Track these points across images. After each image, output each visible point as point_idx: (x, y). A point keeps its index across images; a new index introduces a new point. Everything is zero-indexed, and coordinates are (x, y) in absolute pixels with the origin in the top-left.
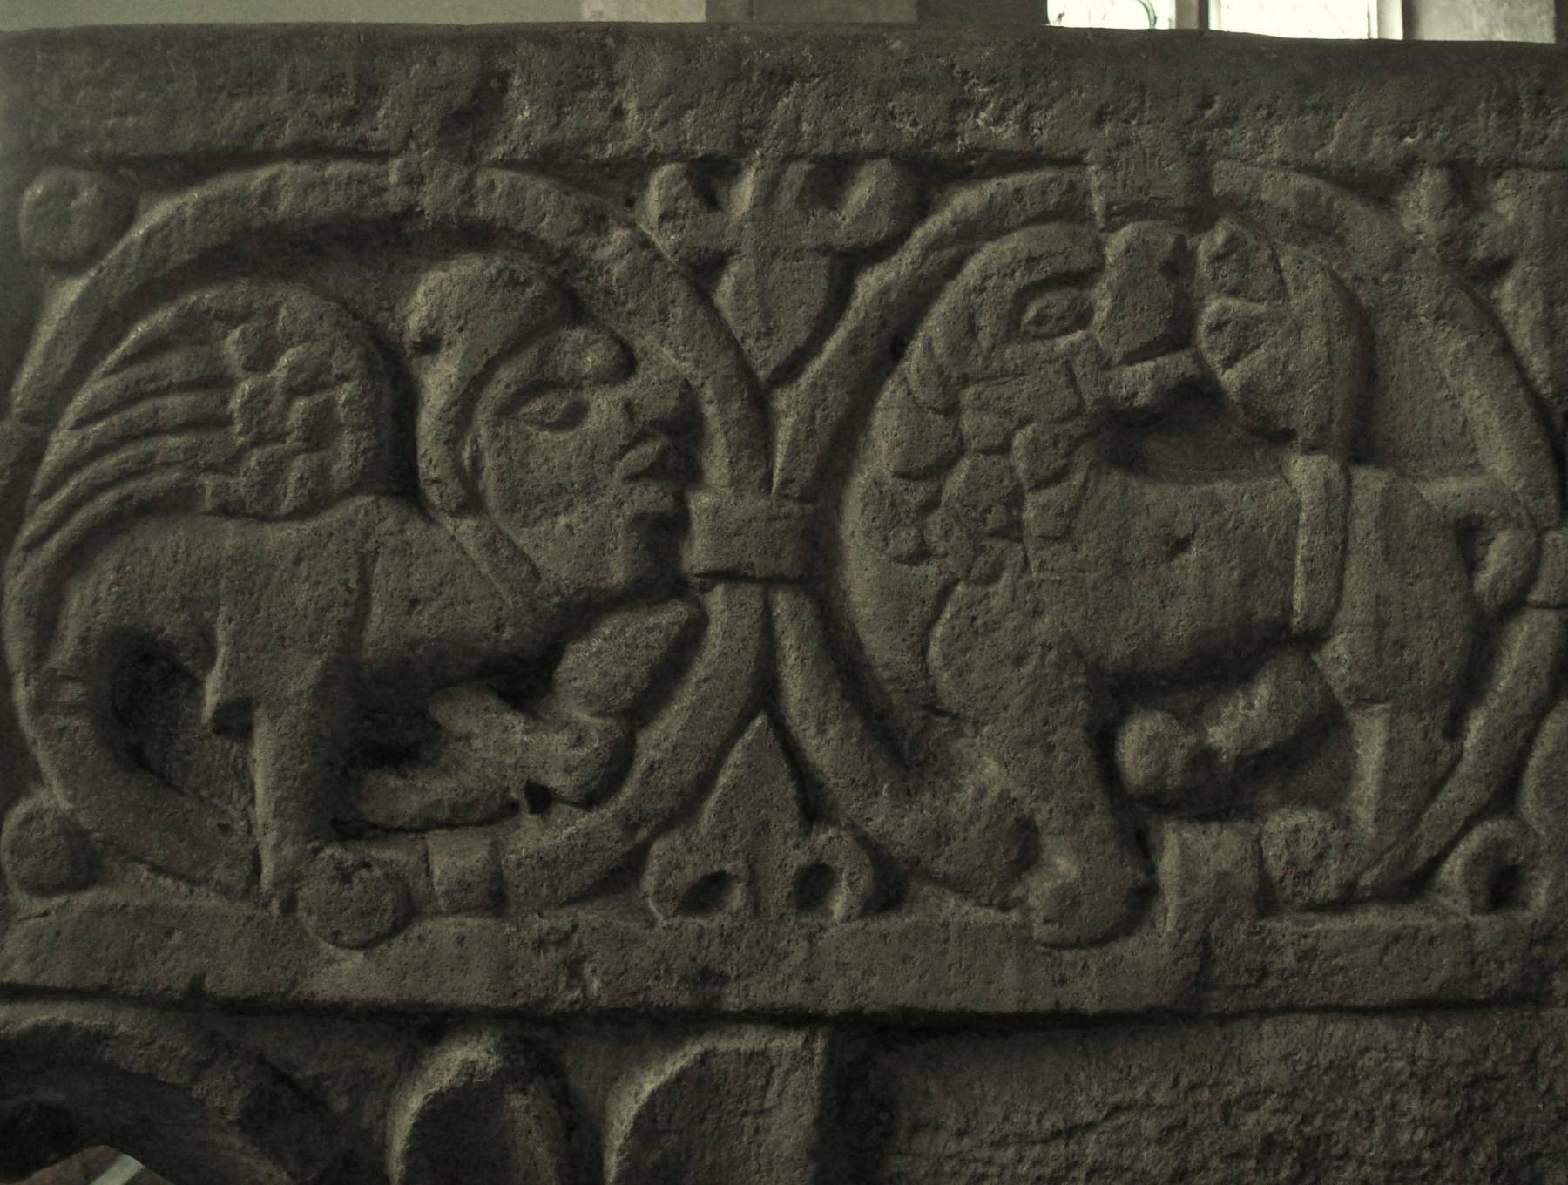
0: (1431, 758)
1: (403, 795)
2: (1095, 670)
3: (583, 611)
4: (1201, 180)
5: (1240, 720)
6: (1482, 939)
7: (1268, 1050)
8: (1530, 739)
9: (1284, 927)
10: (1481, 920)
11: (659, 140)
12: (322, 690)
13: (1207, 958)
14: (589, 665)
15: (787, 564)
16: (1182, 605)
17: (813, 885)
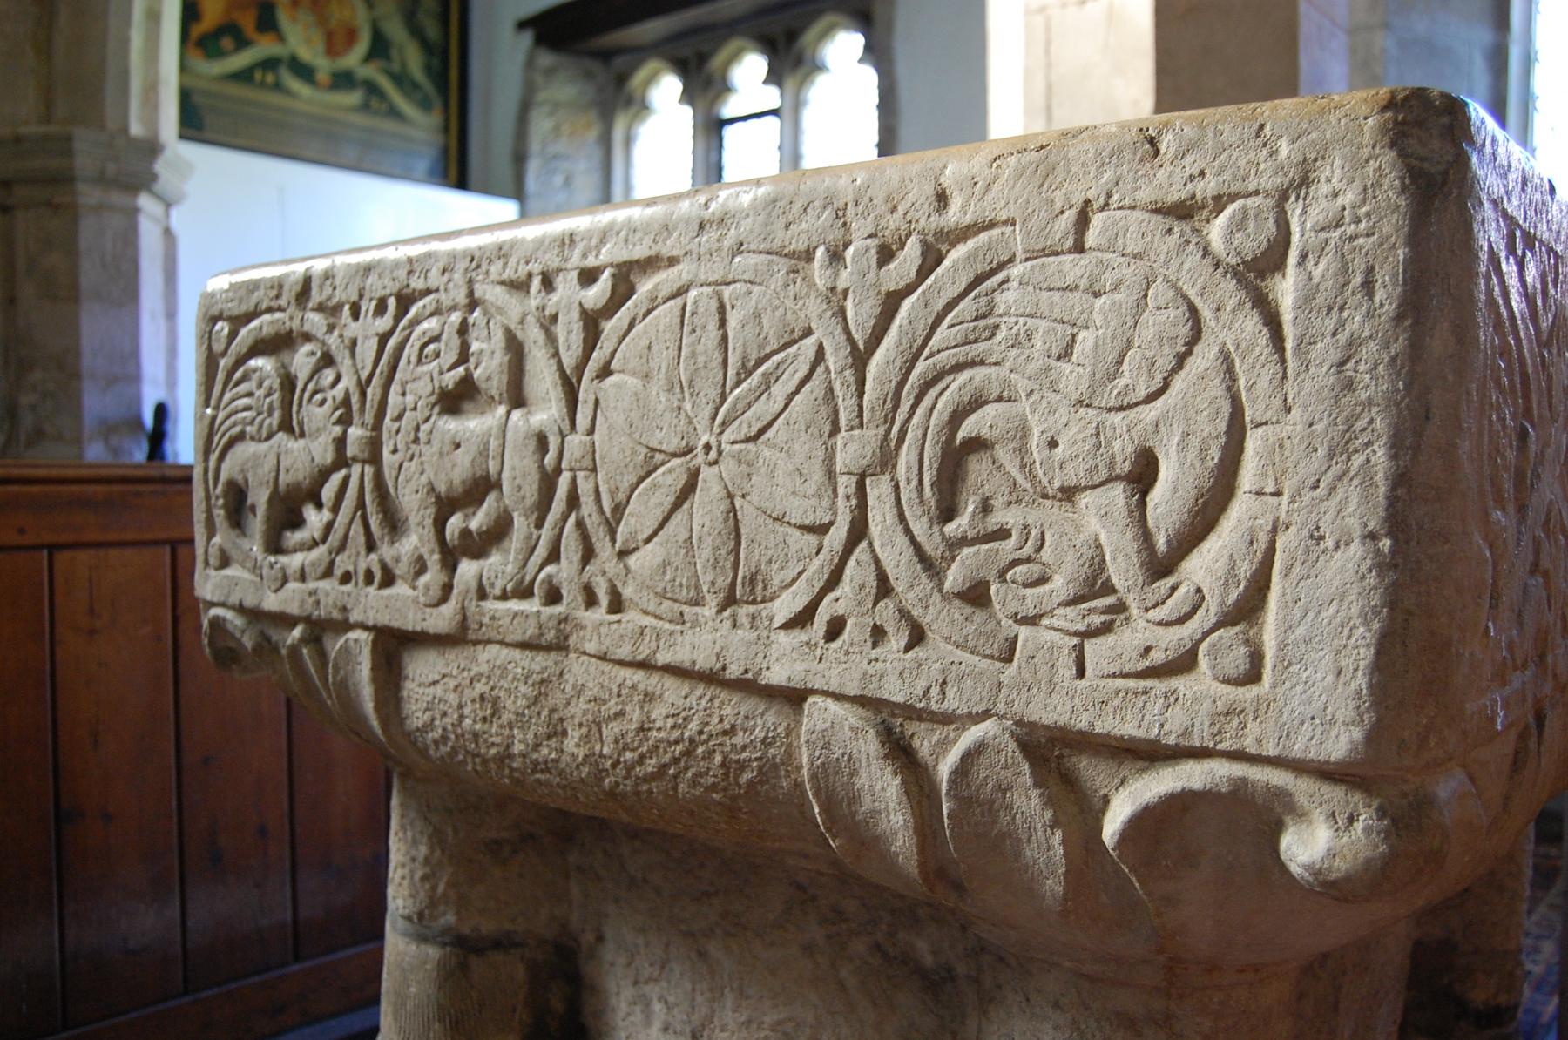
0: (529, 536)
1: (294, 537)
2: (438, 497)
3: (324, 475)
4: (471, 293)
5: (478, 520)
6: (543, 618)
7: (490, 655)
8: (562, 529)
9: (490, 605)
10: (543, 609)
11: (344, 298)
12: (270, 501)
13: (465, 618)
14: (328, 492)
15: (366, 455)
16: (459, 469)
17: (878, 634)
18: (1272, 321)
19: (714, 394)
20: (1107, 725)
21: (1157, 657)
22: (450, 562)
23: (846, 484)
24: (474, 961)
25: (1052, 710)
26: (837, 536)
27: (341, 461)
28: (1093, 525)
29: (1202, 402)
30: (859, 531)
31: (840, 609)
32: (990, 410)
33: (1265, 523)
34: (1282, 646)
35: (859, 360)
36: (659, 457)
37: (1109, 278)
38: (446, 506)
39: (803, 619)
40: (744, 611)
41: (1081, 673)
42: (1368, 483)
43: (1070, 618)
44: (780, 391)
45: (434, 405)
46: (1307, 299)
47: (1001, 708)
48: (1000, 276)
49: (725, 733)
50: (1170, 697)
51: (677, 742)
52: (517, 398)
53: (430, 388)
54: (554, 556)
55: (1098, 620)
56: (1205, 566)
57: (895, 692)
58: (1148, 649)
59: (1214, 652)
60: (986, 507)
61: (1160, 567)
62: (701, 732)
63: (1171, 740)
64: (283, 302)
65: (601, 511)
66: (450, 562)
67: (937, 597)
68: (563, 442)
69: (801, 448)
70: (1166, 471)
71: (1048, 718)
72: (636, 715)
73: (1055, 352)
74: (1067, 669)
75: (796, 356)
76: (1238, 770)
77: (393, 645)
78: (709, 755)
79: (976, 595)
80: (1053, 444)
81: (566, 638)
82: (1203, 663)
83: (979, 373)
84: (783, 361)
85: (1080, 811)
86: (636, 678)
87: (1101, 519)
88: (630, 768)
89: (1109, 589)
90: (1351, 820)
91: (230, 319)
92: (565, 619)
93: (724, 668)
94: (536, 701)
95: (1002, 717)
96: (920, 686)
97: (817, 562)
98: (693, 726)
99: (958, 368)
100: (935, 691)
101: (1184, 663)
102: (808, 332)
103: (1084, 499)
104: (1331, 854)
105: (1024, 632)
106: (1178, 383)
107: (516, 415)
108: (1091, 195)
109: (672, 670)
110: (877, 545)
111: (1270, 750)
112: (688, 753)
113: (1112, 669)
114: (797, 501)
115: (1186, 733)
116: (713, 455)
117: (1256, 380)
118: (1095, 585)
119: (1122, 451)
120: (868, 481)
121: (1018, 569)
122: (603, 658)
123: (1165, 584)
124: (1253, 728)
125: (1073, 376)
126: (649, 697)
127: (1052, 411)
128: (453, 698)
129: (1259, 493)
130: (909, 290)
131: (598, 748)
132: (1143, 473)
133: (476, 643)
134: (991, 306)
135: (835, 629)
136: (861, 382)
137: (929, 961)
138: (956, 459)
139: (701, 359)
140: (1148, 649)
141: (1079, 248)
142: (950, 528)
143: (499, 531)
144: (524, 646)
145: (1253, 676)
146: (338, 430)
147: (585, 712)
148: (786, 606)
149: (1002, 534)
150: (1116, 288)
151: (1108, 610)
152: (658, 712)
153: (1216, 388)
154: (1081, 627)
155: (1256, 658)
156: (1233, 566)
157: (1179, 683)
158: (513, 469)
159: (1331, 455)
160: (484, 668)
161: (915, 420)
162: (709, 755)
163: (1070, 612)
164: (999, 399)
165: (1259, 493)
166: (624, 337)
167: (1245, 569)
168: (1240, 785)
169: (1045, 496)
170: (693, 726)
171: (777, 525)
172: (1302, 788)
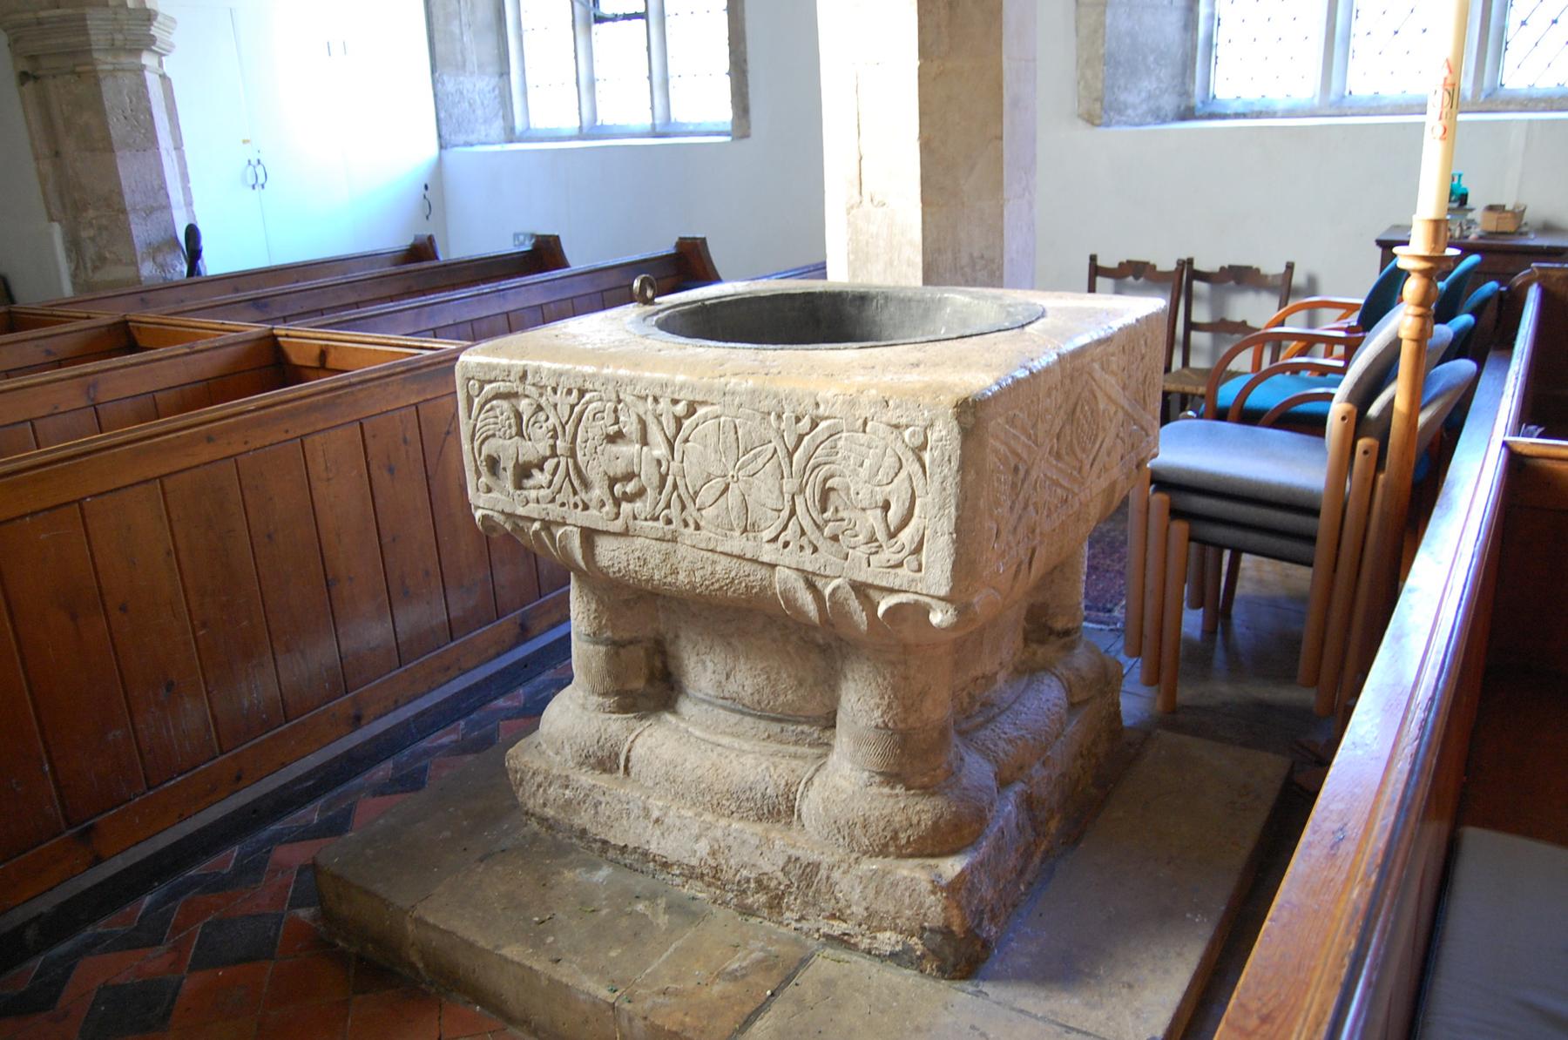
3: (545, 459)
23: (787, 497)
24: (622, 651)
26: (785, 513)
28: (871, 520)
30: (793, 513)
35: (790, 455)
38: (613, 482)
40: (751, 535)
44: (760, 461)
50: (896, 575)
54: (668, 506)
56: (905, 536)
60: (837, 510)
61: (892, 535)
66: (617, 503)
69: (770, 481)
83: (833, 467)
87: (873, 518)
117: (918, 483)
118: (872, 539)
119: (880, 499)
125: (864, 472)
128: (624, 557)
132: (886, 506)
135: (786, 545)
143: (641, 493)
145: (920, 570)
146: (551, 442)
167: (917, 539)
172: (933, 602)
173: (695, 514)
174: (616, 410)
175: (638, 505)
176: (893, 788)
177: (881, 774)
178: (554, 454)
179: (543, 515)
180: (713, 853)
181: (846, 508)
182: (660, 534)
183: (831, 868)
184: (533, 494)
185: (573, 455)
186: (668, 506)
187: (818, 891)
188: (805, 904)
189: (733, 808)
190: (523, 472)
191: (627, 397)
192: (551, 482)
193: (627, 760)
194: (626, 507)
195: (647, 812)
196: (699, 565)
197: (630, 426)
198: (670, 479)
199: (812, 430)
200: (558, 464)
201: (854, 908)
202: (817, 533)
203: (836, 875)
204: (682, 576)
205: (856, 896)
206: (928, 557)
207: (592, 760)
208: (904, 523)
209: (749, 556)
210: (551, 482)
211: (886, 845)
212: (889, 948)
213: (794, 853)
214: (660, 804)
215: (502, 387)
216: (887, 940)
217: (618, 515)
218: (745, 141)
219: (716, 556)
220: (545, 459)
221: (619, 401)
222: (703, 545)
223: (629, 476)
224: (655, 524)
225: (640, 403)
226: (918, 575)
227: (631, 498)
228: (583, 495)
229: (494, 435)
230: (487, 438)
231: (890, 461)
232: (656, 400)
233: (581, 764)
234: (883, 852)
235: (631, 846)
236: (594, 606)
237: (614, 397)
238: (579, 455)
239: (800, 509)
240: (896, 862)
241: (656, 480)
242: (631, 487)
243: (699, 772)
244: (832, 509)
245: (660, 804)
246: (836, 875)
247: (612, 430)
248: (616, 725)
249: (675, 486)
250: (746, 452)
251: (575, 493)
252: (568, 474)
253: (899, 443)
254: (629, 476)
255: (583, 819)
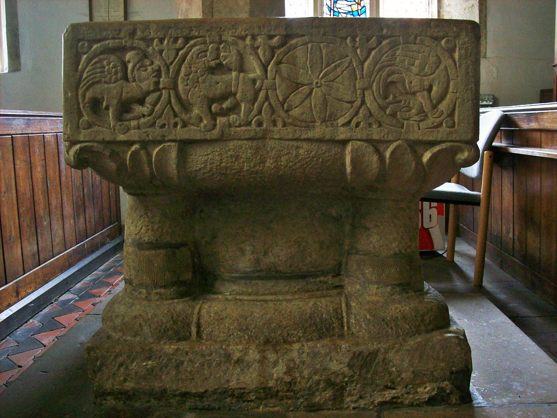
0: (250, 108)
3: (148, 93)
5: (226, 104)
13: (223, 134)
15: (171, 87)
18: (454, 61)
19: (319, 70)
20: (425, 138)
21: (435, 124)
22: (214, 116)
23: (359, 92)
24: (177, 251)
25: (413, 136)
26: (358, 102)
27: (157, 89)
28: (420, 99)
29: (442, 75)
30: (363, 102)
31: (359, 120)
32: (396, 76)
33: (454, 98)
34: (459, 120)
35: (362, 63)
36: (299, 86)
37: (422, 50)
38: (212, 101)
39: (348, 123)
40: (328, 123)
41: (419, 129)
42: (472, 91)
43: (416, 118)
44: (339, 70)
45: (205, 71)
46: (460, 56)
47: (402, 137)
48: (397, 47)
49: (323, 153)
50: (438, 132)
51: (308, 158)
52: (241, 69)
53: (204, 66)
54: (260, 112)
55: (423, 118)
56: (443, 106)
57: (375, 137)
58: (433, 123)
59: (446, 122)
60: (395, 97)
61: (435, 107)
62: (315, 154)
63: (439, 139)
64: (122, 35)
65: (279, 100)
66: (214, 116)
67: (385, 116)
68: (263, 82)
69: (346, 83)
70: (435, 89)
71: (412, 138)
72: (294, 153)
73: (411, 64)
74: (416, 128)
75: (344, 62)
76: (452, 144)
77: (185, 145)
78: (318, 160)
79: (393, 115)
80: (411, 83)
81: (266, 135)
82: (444, 125)
83: (393, 68)
84: (341, 62)
85: (418, 158)
86: (293, 143)
87: (421, 99)
88: (290, 167)
89: (424, 112)
90: (471, 150)
91: (89, 41)
92: (266, 130)
93: (324, 137)
94: (255, 154)
95: (403, 139)
96: (382, 135)
97: (352, 110)
98: (313, 153)
99: (388, 66)
100: (386, 136)
101: (440, 125)
102: (347, 56)
103: (418, 94)
104: (468, 156)
105: (405, 122)
106: (437, 71)
107: (242, 75)
108: (418, 32)
109: (305, 140)
110: (368, 105)
111: (458, 139)
112: (311, 160)
113: (426, 127)
114: (346, 96)
115: (442, 138)
116: (319, 85)
117: (452, 72)
118: (421, 111)
119: (426, 83)
120: (365, 91)
121: (405, 108)
122: (281, 139)
123: (435, 110)
124: (454, 135)
125: (415, 69)
126: (298, 148)
127: (410, 76)
128: (218, 158)
129: (453, 92)
130: (374, 49)
131: (279, 163)
132: (430, 89)
133: (226, 141)
134: (395, 54)
135: (358, 125)
136: (363, 68)
137: (335, 214)
138: (388, 86)
139: (314, 61)
140: (433, 123)
141: (415, 43)
142: (387, 101)
143: (235, 108)
144: (247, 139)
145: (453, 126)
146: (155, 79)
147: (275, 154)
148: (341, 121)
149: (400, 101)
150: (424, 52)
151: (424, 116)
152: (301, 151)
153: (444, 73)
154: (419, 120)
155: (454, 123)
156: (449, 107)
157: (440, 129)
158: (243, 89)
159: (465, 86)
160: (232, 147)
161: (377, 77)
162: (318, 160)
163: (417, 117)
164: (397, 73)
165: (453, 92)
166: (286, 54)
167: (451, 106)
168: (452, 146)
169: (408, 94)
170: (313, 153)
171: (339, 102)
172: (463, 145)
173: (283, 115)
174: (218, 49)
175: (233, 117)
176: (407, 293)
177: (399, 285)
178: (157, 89)
179: (144, 137)
180: (289, 371)
181: (401, 94)
182: (252, 134)
183: (387, 352)
184: (133, 123)
185: (175, 87)
186: (260, 112)
187: (376, 373)
188: (364, 385)
189: (300, 334)
190: (125, 108)
191: (228, 37)
192: (152, 111)
193: (199, 326)
194: (221, 120)
195: (228, 356)
196: (286, 151)
197: (229, 57)
198: (262, 94)
199: (378, 46)
200: (161, 95)
201: (404, 375)
202: (382, 113)
203: (391, 355)
204: (269, 163)
205: (406, 364)
206: (459, 116)
207: (170, 333)
208: (442, 98)
209: (328, 137)
210: (152, 111)
211: (419, 326)
212: (427, 396)
213: (357, 349)
214: (240, 347)
215: (110, 43)
216: (426, 391)
217: (215, 125)
218: (17, 74)
219: (299, 143)
220: (148, 93)
221: (221, 42)
222: (290, 136)
223: (223, 98)
224: (249, 128)
225: (240, 42)
226: (453, 129)
227: (225, 113)
228: (184, 117)
229: (98, 82)
230: (93, 84)
231: (432, 59)
232: (254, 38)
233: (159, 338)
234: (418, 332)
235: (210, 389)
236: (157, 219)
237: (217, 39)
238: (180, 87)
239: (368, 101)
240: (428, 336)
241: (250, 95)
242: (226, 104)
243: (268, 317)
244: (391, 96)
245: (240, 347)
246: (391, 355)
247: (213, 63)
248: (180, 306)
249: (267, 98)
250: (328, 65)
251: (175, 116)
252: (170, 102)
253: (439, 48)
254: (223, 98)
255: (167, 381)
